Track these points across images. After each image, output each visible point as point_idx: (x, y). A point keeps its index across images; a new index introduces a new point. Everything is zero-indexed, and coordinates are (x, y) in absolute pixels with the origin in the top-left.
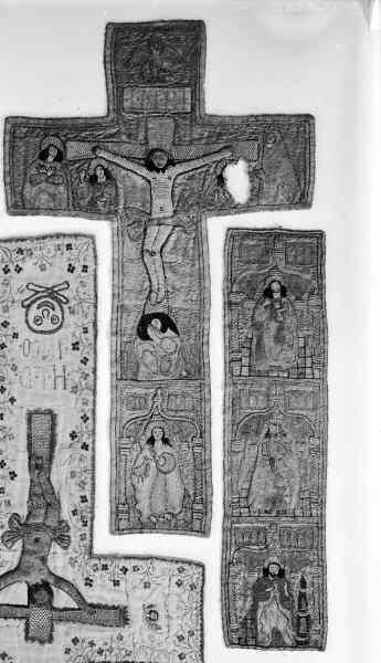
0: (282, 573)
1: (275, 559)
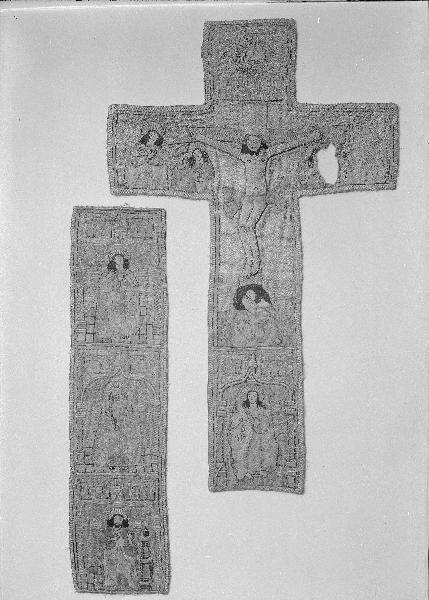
0: (125, 524)
1: (120, 512)
